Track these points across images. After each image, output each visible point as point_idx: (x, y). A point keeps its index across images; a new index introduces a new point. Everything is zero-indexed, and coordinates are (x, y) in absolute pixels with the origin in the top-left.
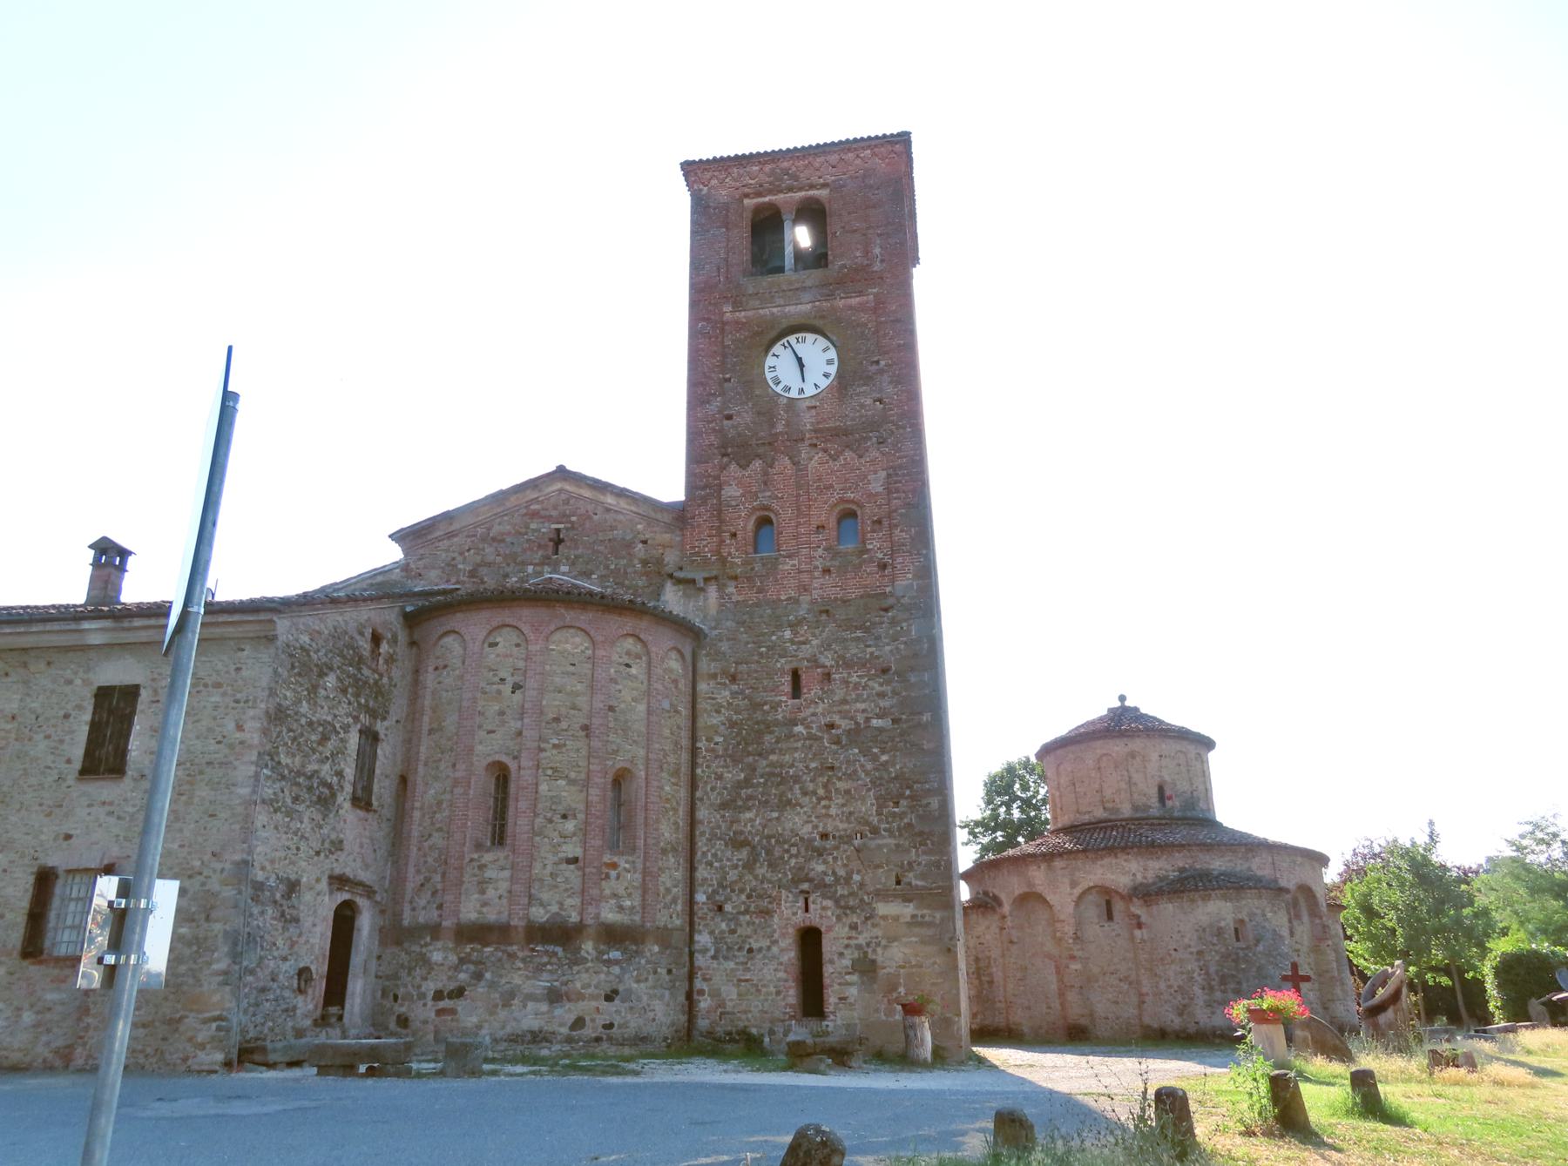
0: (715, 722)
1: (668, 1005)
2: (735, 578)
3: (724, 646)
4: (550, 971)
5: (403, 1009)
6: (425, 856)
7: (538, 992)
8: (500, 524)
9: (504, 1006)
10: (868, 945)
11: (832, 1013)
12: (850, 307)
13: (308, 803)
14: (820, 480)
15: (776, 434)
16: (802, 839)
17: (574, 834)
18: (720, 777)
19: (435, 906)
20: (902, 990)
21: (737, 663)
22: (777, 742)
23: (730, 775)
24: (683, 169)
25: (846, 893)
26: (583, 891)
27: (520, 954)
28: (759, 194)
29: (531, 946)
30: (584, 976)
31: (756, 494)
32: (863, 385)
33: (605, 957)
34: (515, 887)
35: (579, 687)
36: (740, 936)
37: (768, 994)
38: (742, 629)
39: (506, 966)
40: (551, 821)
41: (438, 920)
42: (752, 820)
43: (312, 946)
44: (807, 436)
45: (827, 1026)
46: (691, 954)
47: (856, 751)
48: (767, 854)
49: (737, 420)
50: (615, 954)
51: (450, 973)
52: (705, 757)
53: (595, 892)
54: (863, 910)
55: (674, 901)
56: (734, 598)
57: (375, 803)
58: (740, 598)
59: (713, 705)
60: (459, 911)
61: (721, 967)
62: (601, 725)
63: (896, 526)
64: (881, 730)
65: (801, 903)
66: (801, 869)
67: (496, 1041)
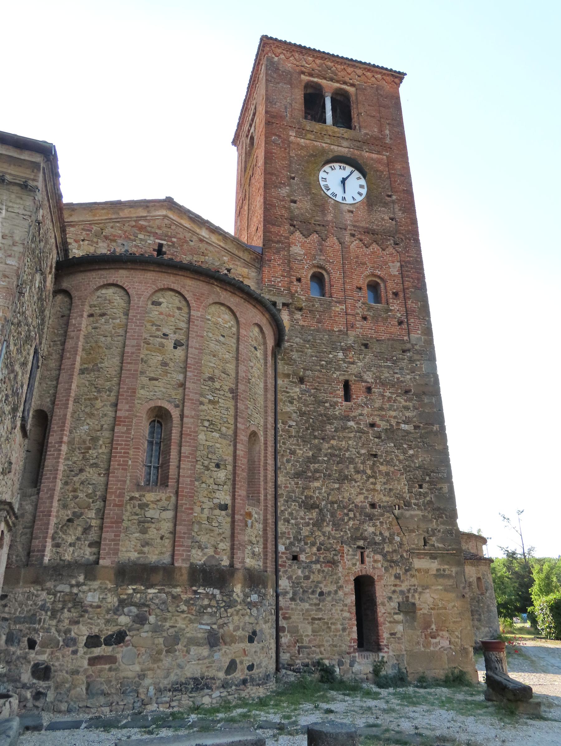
0: (288, 410)
2: (300, 309)
3: (295, 355)
5: (44, 657)
6: (75, 490)
7: (199, 635)
8: (112, 228)
9: (167, 651)
10: (409, 591)
11: (386, 645)
12: (372, 159)
14: (357, 257)
15: (327, 221)
16: (356, 506)
17: (225, 483)
18: (293, 453)
20: (433, 626)
21: (304, 369)
24: (261, 39)
25: (391, 550)
28: (311, 75)
29: (194, 588)
30: (236, 618)
31: (314, 256)
32: (383, 207)
33: (249, 600)
36: (313, 582)
37: (337, 630)
39: (170, 609)
40: (207, 468)
44: (349, 228)
45: (383, 657)
47: (392, 445)
48: (332, 516)
49: (299, 205)
50: (254, 597)
51: (108, 617)
54: (403, 564)
56: (301, 323)
58: (305, 324)
59: (288, 397)
61: (299, 608)
63: (409, 298)
64: (408, 433)
65: (358, 557)
66: (357, 529)
67: (160, 691)
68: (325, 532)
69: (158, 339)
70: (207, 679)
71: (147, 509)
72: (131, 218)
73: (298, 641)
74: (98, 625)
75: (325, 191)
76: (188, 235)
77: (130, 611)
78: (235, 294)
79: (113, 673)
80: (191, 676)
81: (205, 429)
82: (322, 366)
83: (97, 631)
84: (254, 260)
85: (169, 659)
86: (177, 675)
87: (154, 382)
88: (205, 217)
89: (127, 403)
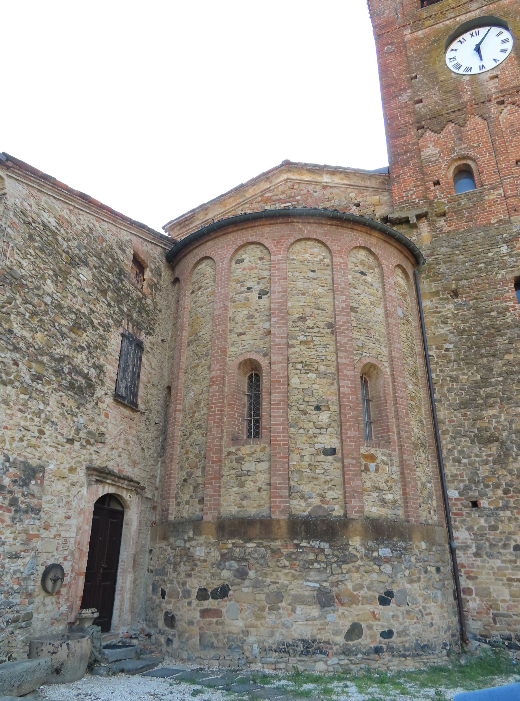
0: (442, 331)
1: (442, 607)
2: (444, 214)
3: (442, 268)
4: (319, 570)
5: (170, 607)
6: (187, 453)
7: (307, 593)
13: (55, 386)
15: (465, 102)
17: (329, 425)
19: (197, 500)
21: (457, 280)
22: (511, 342)
23: (466, 377)
26: (344, 483)
27: (285, 551)
29: (296, 542)
30: (355, 575)
33: (375, 554)
34: (274, 479)
35: (321, 290)
36: (503, 533)
38: (457, 252)
39: (270, 564)
40: (304, 413)
41: (200, 514)
42: (495, 416)
43: (66, 541)
46: (452, 551)
49: (425, 102)
50: (385, 552)
51: (213, 570)
52: (437, 363)
53: (356, 484)
55: (430, 496)
56: (446, 229)
57: (141, 406)
59: (440, 318)
60: (219, 505)
61: (487, 565)
62: (345, 322)
67: (264, 650)
68: (512, 470)
69: (242, 295)
70: (320, 643)
71: (243, 463)
72: (256, 194)
73: (491, 606)
74: (205, 579)
75: (456, 71)
76: (311, 188)
77: (231, 566)
78: (322, 223)
79: (220, 627)
80: (300, 637)
81: (299, 372)
82: (480, 269)
83: (204, 584)
84: (383, 183)
85: (273, 617)
86: (282, 634)
87: (242, 337)
88: (322, 163)
89: (218, 363)
